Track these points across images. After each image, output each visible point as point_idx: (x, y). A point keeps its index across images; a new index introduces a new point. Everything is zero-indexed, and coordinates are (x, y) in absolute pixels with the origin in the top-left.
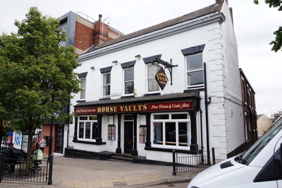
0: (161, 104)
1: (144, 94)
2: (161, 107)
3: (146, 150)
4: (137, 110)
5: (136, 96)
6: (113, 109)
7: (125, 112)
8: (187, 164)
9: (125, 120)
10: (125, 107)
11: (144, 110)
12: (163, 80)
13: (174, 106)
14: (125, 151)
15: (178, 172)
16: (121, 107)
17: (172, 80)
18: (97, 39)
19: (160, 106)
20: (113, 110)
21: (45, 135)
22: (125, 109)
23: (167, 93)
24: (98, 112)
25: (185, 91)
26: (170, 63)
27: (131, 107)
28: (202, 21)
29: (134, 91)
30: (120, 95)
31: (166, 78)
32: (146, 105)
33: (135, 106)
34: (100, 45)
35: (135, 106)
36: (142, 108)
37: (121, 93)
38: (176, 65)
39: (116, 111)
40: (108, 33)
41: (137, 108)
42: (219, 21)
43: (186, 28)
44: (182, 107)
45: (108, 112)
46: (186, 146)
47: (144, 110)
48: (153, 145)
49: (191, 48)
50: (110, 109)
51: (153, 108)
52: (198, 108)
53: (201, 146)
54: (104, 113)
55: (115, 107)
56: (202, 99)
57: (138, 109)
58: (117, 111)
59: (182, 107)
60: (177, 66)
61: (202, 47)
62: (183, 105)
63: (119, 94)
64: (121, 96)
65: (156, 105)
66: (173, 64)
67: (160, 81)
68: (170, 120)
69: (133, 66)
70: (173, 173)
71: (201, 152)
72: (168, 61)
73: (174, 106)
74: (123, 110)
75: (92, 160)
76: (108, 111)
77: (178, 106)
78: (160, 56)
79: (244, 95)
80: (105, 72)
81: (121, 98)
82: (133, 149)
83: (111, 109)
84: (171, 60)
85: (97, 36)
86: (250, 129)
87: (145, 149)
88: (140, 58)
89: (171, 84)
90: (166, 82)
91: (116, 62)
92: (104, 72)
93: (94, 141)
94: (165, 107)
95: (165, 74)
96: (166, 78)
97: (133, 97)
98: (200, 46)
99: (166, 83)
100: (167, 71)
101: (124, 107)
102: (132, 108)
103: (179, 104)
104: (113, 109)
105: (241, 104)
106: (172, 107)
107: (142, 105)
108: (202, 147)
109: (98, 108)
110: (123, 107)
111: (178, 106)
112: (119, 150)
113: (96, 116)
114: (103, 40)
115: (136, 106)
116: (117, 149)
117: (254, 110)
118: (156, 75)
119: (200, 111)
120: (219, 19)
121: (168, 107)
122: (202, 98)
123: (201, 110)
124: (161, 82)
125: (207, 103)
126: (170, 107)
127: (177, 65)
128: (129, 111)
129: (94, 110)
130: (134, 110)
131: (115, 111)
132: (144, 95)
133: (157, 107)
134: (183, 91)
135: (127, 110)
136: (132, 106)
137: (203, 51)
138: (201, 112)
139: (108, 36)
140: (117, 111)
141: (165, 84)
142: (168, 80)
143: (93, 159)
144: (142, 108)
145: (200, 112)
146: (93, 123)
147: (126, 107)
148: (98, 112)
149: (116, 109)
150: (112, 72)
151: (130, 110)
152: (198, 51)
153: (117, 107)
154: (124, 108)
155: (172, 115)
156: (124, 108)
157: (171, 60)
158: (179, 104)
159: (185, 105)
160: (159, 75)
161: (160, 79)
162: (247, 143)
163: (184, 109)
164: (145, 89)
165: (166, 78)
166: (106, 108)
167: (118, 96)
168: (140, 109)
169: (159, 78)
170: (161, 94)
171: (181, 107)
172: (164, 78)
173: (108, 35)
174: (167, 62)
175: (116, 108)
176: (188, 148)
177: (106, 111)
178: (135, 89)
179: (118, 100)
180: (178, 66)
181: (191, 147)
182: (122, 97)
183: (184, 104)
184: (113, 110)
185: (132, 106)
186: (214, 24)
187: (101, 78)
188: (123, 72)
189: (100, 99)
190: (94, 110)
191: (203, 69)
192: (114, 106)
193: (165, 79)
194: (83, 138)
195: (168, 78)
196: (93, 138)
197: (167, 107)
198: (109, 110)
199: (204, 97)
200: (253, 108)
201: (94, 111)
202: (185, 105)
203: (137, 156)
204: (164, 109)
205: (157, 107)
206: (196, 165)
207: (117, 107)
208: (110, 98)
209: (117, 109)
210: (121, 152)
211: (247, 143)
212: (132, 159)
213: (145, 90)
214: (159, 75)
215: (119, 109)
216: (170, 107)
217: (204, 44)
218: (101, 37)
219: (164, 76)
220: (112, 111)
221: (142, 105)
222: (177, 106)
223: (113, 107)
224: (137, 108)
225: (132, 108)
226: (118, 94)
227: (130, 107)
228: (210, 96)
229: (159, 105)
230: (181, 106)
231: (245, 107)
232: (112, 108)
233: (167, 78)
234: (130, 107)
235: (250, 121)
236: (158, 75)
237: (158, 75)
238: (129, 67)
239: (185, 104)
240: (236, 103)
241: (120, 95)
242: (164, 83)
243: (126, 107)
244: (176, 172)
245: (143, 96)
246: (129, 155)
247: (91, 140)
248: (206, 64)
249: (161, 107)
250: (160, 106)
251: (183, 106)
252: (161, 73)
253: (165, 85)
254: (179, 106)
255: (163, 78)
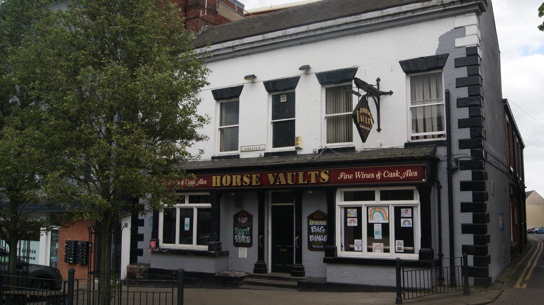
0: (360, 170)
1: (320, 148)
2: (359, 177)
3: (326, 264)
4: (306, 182)
5: (299, 153)
6: (251, 178)
7: (278, 185)
8: (414, 286)
9: (273, 202)
10: (277, 176)
11: (322, 181)
12: (366, 123)
13: (386, 174)
14: (274, 269)
15: (405, 299)
16: (270, 176)
17: (381, 122)
18: (194, 18)
19: (358, 175)
20: (251, 182)
21: (69, 239)
22: (279, 179)
23: (368, 147)
24: (214, 185)
25: (407, 145)
26: (376, 87)
27: (293, 175)
28: (443, 9)
29: (296, 142)
30: (264, 150)
31: (371, 117)
32: (328, 172)
33: (301, 174)
34: (200, 33)
35: (301, 174)
36: (318, 177)
37: (265, 145)
38: (389, 91)
39: (257, 183)
40: (217, 4)
41: (306, 177)
42: (477, 10)
43: (411, 17)
44: (404, 177)
45: (238, 186)
46: (412, 252)
47: (322, 181)
48: (342, 253)
49: (420, 58)
50: (242, 179)
51: (343, 177)
52: (433, 179)
53: (438, 252)
54: (227, 188)
55: (254, 176)
56: (441, 161)
57: (309, 180)
58: (259, 184)
59: (403, 177)
60: (391, 93)
61: (442, 58)
62: (406, 173)
63: (261, 146)
64: (266, 152)
65: (348, 172)
66: (382, 89)
67: (360, 125)
68: (187, 204)
69: (441, 68)
70: (397, 299)
71: (439, 264)
72: (372, 82)
73: (386, 174)
74: (275, 182)
75: (198, 289)
76: (239, 184)
77: (396, 174)
78: (354, 70)
79: (509, 151)
80: (225, 97)
81: (265, 156)
82: (294, 263)
83: (246, 179)
84: (378, 80)
85: (193, 11)
86: (516, 222)
87: (325, 261)
88: (310, 72)
89: (379, 130)
90: (370, 126)
91: (253, 77)
92: (222, 98)
93: (204, 248)
94: (368, 176)
95: (369, 111)
96: (370, 118)
97: (294, 153)
98: (439, 57)
99: (371, 128)
100: (371, 101)
101: (275, 174)
102: (295, 178)
103: (397, 171)
104: (251, 178)
105: (505, 169)
106: (382, 176)
107: (317, 173)
108: (441, 255)
109: (214, 178)
110: (273, 175)
111: (396, 174)
112: (260, 267)
113: (208, 194)
114: (207, 22)
115: (304, 174)
116: (255, 265)
117: (522, 182)
118: (355, 112)
119: (436, 184)
120: (477, 8)
121: (375, 176)
122: (441, 160)
123: (439, 183)
124: (363, 127)
125: (451, 168)
126: (379, 175)
127: (391, 91)
128: (287, 184)
129: (202, 182)
130: (301, 181)
131: (254, 183)
132: (320, 150)
133: (350, 177)
134: (404, 145)
135: (283, 182)
136: (296, 174)
137: (444, 66)
138: (439, 188)
139: (217, 12)
140: (259, 184)
141: (369, 129)
142: (373, 122)
143: (201, 288)
144: (318, 177)
145: (437, 186)
146: (341, 207)
147: (281, 175)
148: (214, 185)
149: (257, 180)
150: (243, 98)
151: (290, 182)
152: (434, 66)
153: (259, 175)
154: (276, 178)
155: (382, 192)
156: (276, 178)
157: (378, 80)
158: (397, 171)
159: (409, 173)
160: (359, 112)
161: (362, 121)
162: (514, 247)
163: (409, 181)
164: (321, 138)
165: (370, 118)
166: (234, 177)
167: (253, 151)
168: (313, 181)
169: (360, 118)
170: (356, 149)
171: (401, 177)
172: (367, 119)
173: (217, 10)
174: (371, 85)
175: (257, 176)
176: (415, 257)
177: (234, 184)
178: (298, 138)
179: (260, 158)
180: (392, 95)
181: (421, 253)
182: (267, 155)
183: (408, 171)
184: (251, 182)
185: (295, 173)
186: (467, 16)
187: (216, 110)
188: (268, 100)
189: (213, 158)
190: (202, 182)
191: (444, 102)
192: (253, 174)
193: (369, 119)
194: (174, 243)
195: (373, 118)
196: (198, 243)
197: (373, 176)
198: (242, 182)
199: (446, 158)
200: (520, 179)
201: (202, 183)
202: (409, 173)
203: (304, 278)
204: (366, 180)
205: (350, 177)
206: (429, 288)
207: (259, 175)
208: (239, 155)
209: (259, 179)
210: (266, 271)
211: (514, 247)
212: (295, 283)
213: (321, 141)
214: (360, 112)
215: (263, 179)
216: (379, 175)
217: (444, 54)
218: (203, 13)
219: (367, 115)
220: (248, 183)
221: (317, 173)
222: (392, 175)
223: (249, 176)
224: (306, 177)
225: (295, 178)
226: (259, 147)
227: (289, 175)
228: (456, 157)
229: (356, 173)
230: (401, 174)
231: (511, 177)
232: (247, 176)
233: (372, 117)
234: (289, 175)
235: (516, 204)
236: (357, 111)
237: (357, 111)
238: (283, 89)
239: (410, 170)
240: (500, 169)
241: (261, 149)
242: (366, 128)
243: (281, 175)
244: (402, 298)
245: (317, 152)
246: (284, 276)
247: (194, 246)
248: (450, 92)
249: (359, 177)
250: (358, 175)
251: (406, 175)
252: (364, 109)
253: (369, 131)
254: (397, 174)
255: (366, 118)
